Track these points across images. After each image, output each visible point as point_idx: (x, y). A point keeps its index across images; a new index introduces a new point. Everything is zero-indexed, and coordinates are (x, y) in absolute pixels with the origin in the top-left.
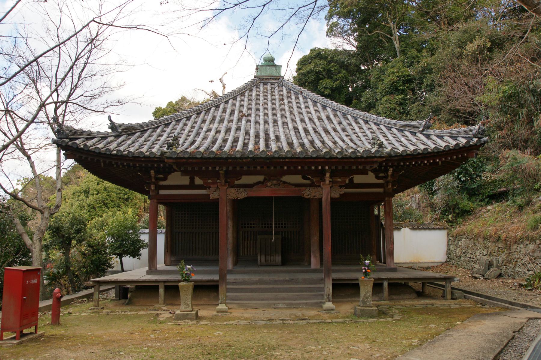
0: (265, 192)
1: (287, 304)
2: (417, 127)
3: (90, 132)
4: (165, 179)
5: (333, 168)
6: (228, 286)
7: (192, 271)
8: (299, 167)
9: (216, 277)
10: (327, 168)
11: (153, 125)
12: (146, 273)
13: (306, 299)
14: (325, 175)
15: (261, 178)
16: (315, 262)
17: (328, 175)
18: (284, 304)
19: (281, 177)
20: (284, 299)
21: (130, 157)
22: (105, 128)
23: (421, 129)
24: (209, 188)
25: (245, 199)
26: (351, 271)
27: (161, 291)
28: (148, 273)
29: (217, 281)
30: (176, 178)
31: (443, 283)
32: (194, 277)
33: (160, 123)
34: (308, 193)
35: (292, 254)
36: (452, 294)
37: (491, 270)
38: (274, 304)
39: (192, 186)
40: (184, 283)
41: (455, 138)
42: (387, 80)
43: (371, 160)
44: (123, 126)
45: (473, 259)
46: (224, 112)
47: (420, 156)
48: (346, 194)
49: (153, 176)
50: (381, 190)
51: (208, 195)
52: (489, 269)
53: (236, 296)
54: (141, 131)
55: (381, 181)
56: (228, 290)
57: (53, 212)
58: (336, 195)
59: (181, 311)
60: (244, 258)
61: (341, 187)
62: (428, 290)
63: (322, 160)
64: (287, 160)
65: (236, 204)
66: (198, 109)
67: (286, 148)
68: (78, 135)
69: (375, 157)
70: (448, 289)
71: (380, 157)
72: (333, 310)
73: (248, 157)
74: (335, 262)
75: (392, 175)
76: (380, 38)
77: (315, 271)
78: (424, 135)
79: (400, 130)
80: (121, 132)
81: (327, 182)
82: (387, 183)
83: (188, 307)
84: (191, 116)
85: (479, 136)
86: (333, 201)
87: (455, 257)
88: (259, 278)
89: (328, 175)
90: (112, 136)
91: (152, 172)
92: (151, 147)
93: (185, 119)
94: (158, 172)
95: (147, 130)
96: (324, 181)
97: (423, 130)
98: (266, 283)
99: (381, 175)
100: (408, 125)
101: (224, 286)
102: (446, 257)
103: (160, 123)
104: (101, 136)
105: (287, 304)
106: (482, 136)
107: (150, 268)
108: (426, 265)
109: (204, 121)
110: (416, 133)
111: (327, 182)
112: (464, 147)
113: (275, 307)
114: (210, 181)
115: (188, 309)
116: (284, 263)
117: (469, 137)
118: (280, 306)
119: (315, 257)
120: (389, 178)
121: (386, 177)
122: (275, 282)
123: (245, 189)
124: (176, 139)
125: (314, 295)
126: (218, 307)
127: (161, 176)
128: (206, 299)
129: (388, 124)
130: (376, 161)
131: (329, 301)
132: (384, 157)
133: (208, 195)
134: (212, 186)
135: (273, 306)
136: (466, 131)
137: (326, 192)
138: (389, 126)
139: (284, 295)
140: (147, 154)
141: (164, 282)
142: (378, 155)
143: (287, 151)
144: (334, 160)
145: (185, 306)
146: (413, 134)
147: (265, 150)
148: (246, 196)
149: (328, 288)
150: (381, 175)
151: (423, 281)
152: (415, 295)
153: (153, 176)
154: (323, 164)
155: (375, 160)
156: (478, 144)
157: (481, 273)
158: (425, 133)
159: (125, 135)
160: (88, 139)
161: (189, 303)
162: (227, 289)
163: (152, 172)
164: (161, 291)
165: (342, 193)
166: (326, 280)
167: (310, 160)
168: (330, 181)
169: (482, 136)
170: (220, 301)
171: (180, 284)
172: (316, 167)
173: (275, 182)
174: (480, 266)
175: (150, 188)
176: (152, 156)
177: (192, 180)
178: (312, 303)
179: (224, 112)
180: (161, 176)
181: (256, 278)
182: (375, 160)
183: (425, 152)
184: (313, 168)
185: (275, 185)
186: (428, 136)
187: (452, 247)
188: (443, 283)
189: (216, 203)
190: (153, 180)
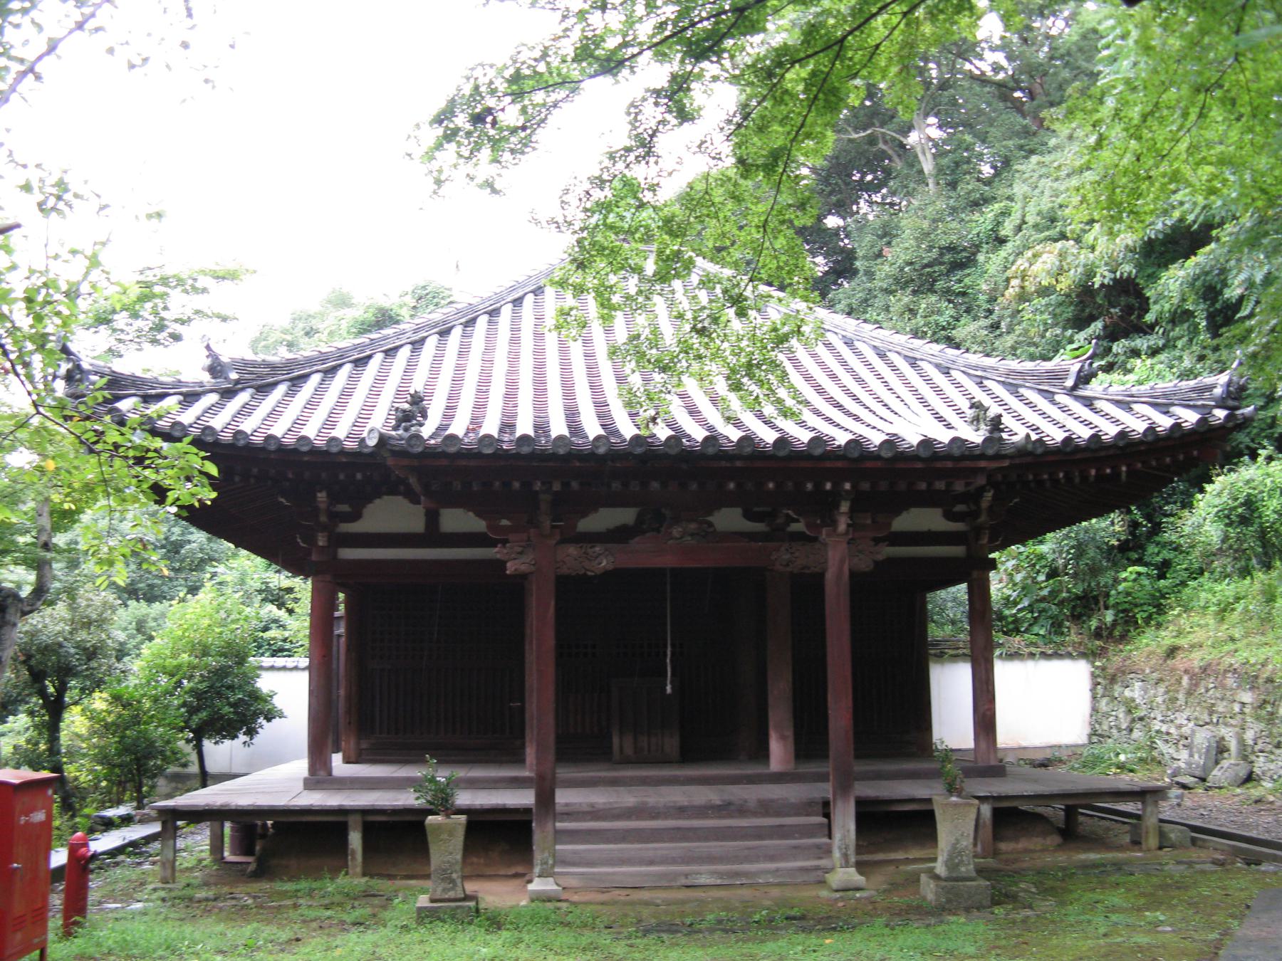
0: (645, 554)
1: (721, 875)
2: (1057, 376)
3: (156, 383)
4: (356, 516)
5: (865, 486)
6: (558, 825)
7: (454, 784)
8: (771, 485)
9: (524, 798)
10: (847, 486)
11: (324, 361)
12: (301, 784)
13: (772, 858)
14: (837, 506)
15: (626, 516)
16: (779, 752)
17: (845, 507)
18: (713, 873)
19: (710, 513)
20: (711, 859)
21: (271, 452)
22: (195, 372)
23: (1070, 383)
24: (504, 542)
25: (607, 573)
26: (879, 776)
27: (355, 839)
28: (312, 783)
29: (527, 811)
30: (391, 514)
31: (1129, 807)
32: (464, 798)
33: (341, 357)
34: (786, 557)
35: (710, 731)
36: (1162, 835)
37: (1225, 763)
38: (686, 876)
39: (432, 536)
40: (439, 818)
41: (1164, 409)
42: (900, 253)
43: (968, 464)
44: (242, 365)
45: (1168, 734)
46: (515, 329)
47: (1079, 456)
48: (891, 561)
49: (323, 506)
50: (957, 551)
51: (501, 564)
52: (1217, 763)
53: (575, 852)
54: (291, 380)
55: (759, 527)
56: (561, 836)
57: (28, 608)
58: (865, 564)
59: (432, 901)
60: (583, 745)
61: (877, 541)
62: (1086, 822)
63: (839, 464)
64: (738, 464)
65: (571, 589)
66: (445, 322)
67: (593, 429)
68: (125, 387)
69: (982, 456)
70: (1151, 822)
71: (998, 457)
72: (858, 889)
73: (630, 454)
74: (861, 754)
75: (990, 508)
76: (881, 146)
77: (779, 778)
78: (1077, 398)
79: (1011, 384)
80: (237, 382)
81: (842, 527)
82: (978, 531)
83: (453, 889)
84: (423, 340)
85: (1231, 403)
86: (860, 584)
87: (1114, 731)
88: (640, 799)
89: (845, 507)
90: (212, 391)
91: (322, 496)
92: (330, 422)
93: (409, 347)
94: (334, 498)
95: (305, 377)
96: (834, 523)
97: (1075, 387)
98: (654, 814)
99: (960, 508)
100: (1031, 374)
101: (549, 826)
102: (1087, 730)
103: (341, 357)
104: (184, 390)
105: (721, 875)
106: (1236, 403)
107: (313, 769)
108: (1039, 756)
109: (463, 352)
110: (1053, 393)
111: (842, 527)
112: (1193, 432)
113: (689, 882)
114: (505, 522)
115: (451, 894)
116: (688, 755)
117: (1203, 406)
118: (703, 880)
119: (782, 738)
120: (983, 518)
121: (974, 515)
122: (681, 811)
123: (609, 545)
124: (417, 400)
125: (795, 847)
126: (531, 887)
127: (344, 508)
128: (475, 860)
129: (976, 368)
130: (983, 469)
131: (846, 864)
132: (1004, 457)
133: (501, 564)
134: (511, 537)
135: (683, 881)
136: (1193, 390)
137: (837, 557)
138: (979, 373)
139: (714, 847)
140: (320, 443)
141: (365, 812)
142: (990, 452)
143: (598, 438)
144: (869, 464)
145: (443, 885)
146: (1048, 395)
147: (602, 432)
148: (610, 567)
149: (845, 824)
150: (960, 508)
151: (1070, 802)
152: (1057, 839)
153: (323, 506)
154: (838, 476)
155: (983, 464)
156: (1230, 424)
157: (1198, 773)
158: (1080, 393)
159: (250, 391)
160: (147, 399)
161: (454, 876)
162: (557, 832)
163: (322, 496)
164: (355, 839)
165: (880, 557)
166: (840, 804)
167: (802, 464)
168: (849, 525)
169: (1236, 403)
170: (537, 870)
171: (431, 819)
172: (818, 486)
173: (693, 526)
174: (1191, 755)
175: (311, 540)
176: (334, 450)
177: (432, 518)
178: (792, 870)
179: (515, 329)
180: (344, 508)
181: (627, 798)
182: (983, 464)
183: (711, 451)
184: (809, 486)
185: (692, 535)
186: (1089, 402)
187: (1103, 705)
188: (1129, 807)
189: (519, 584)
190: (323, 519)
